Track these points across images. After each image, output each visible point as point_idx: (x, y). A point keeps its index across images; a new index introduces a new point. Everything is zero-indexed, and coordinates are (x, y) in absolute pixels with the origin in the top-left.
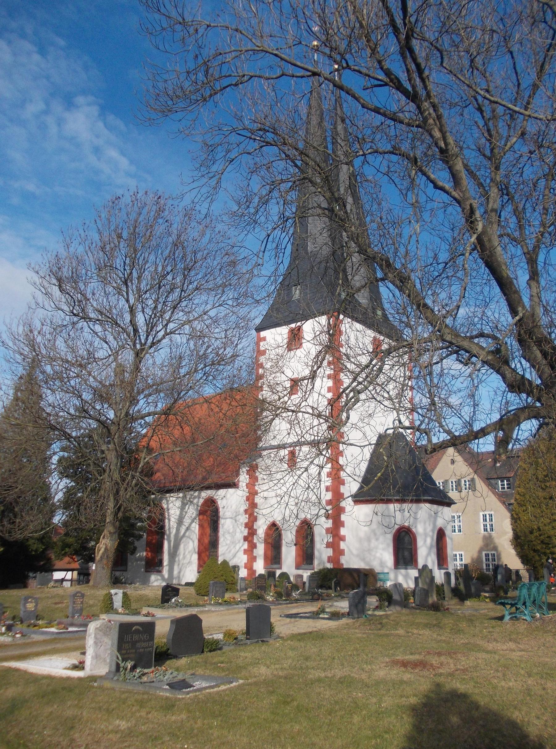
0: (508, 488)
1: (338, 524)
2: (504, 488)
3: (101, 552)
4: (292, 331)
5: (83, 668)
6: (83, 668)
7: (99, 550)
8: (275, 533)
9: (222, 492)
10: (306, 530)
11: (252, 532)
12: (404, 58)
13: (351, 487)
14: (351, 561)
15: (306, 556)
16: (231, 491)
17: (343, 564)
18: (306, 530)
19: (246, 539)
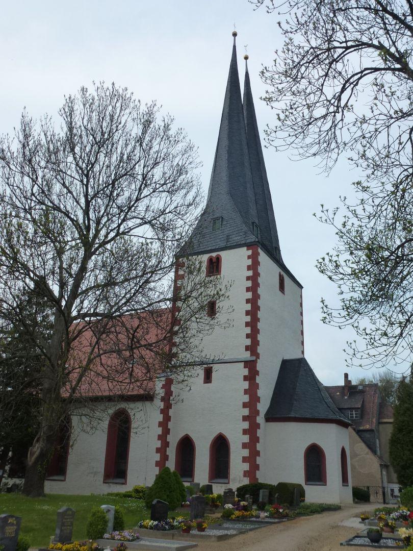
0: (356, 417)
1: (254, 440)
2: (353, 417)
3: (35, 456)
4: (210, 260)
5: (389, 482)
6: (389, 482)
7: (32, 454)
8: (187, 446)
9: (132, 405)
10: (220, 446)
11: (166, 444)
12: (354, 41)
13: (263, 406)
14: (269, 476)
15: (220, 468)
16: (148, 404)
17: (258, 479)
18: (220, 446)
19: (158, 450)
